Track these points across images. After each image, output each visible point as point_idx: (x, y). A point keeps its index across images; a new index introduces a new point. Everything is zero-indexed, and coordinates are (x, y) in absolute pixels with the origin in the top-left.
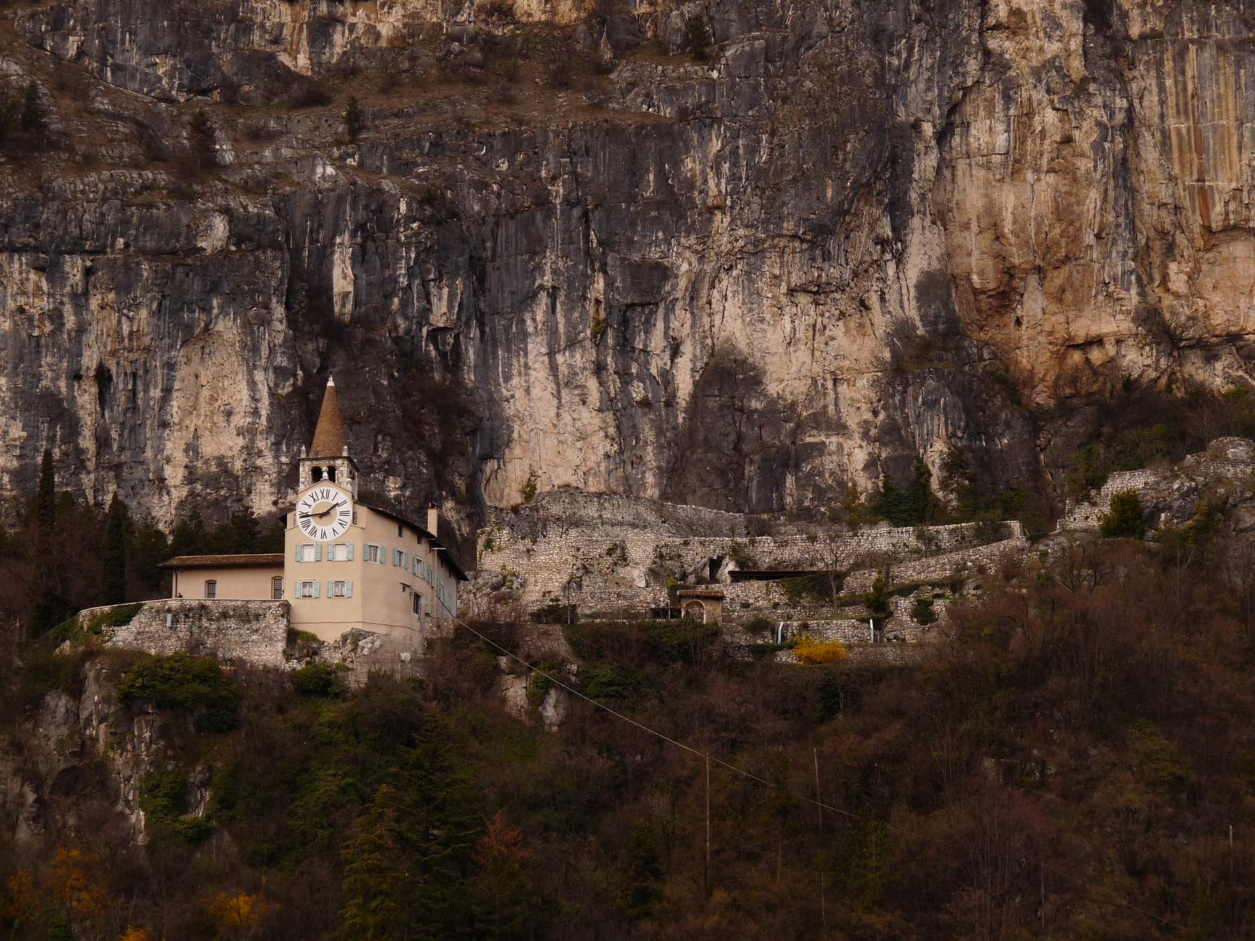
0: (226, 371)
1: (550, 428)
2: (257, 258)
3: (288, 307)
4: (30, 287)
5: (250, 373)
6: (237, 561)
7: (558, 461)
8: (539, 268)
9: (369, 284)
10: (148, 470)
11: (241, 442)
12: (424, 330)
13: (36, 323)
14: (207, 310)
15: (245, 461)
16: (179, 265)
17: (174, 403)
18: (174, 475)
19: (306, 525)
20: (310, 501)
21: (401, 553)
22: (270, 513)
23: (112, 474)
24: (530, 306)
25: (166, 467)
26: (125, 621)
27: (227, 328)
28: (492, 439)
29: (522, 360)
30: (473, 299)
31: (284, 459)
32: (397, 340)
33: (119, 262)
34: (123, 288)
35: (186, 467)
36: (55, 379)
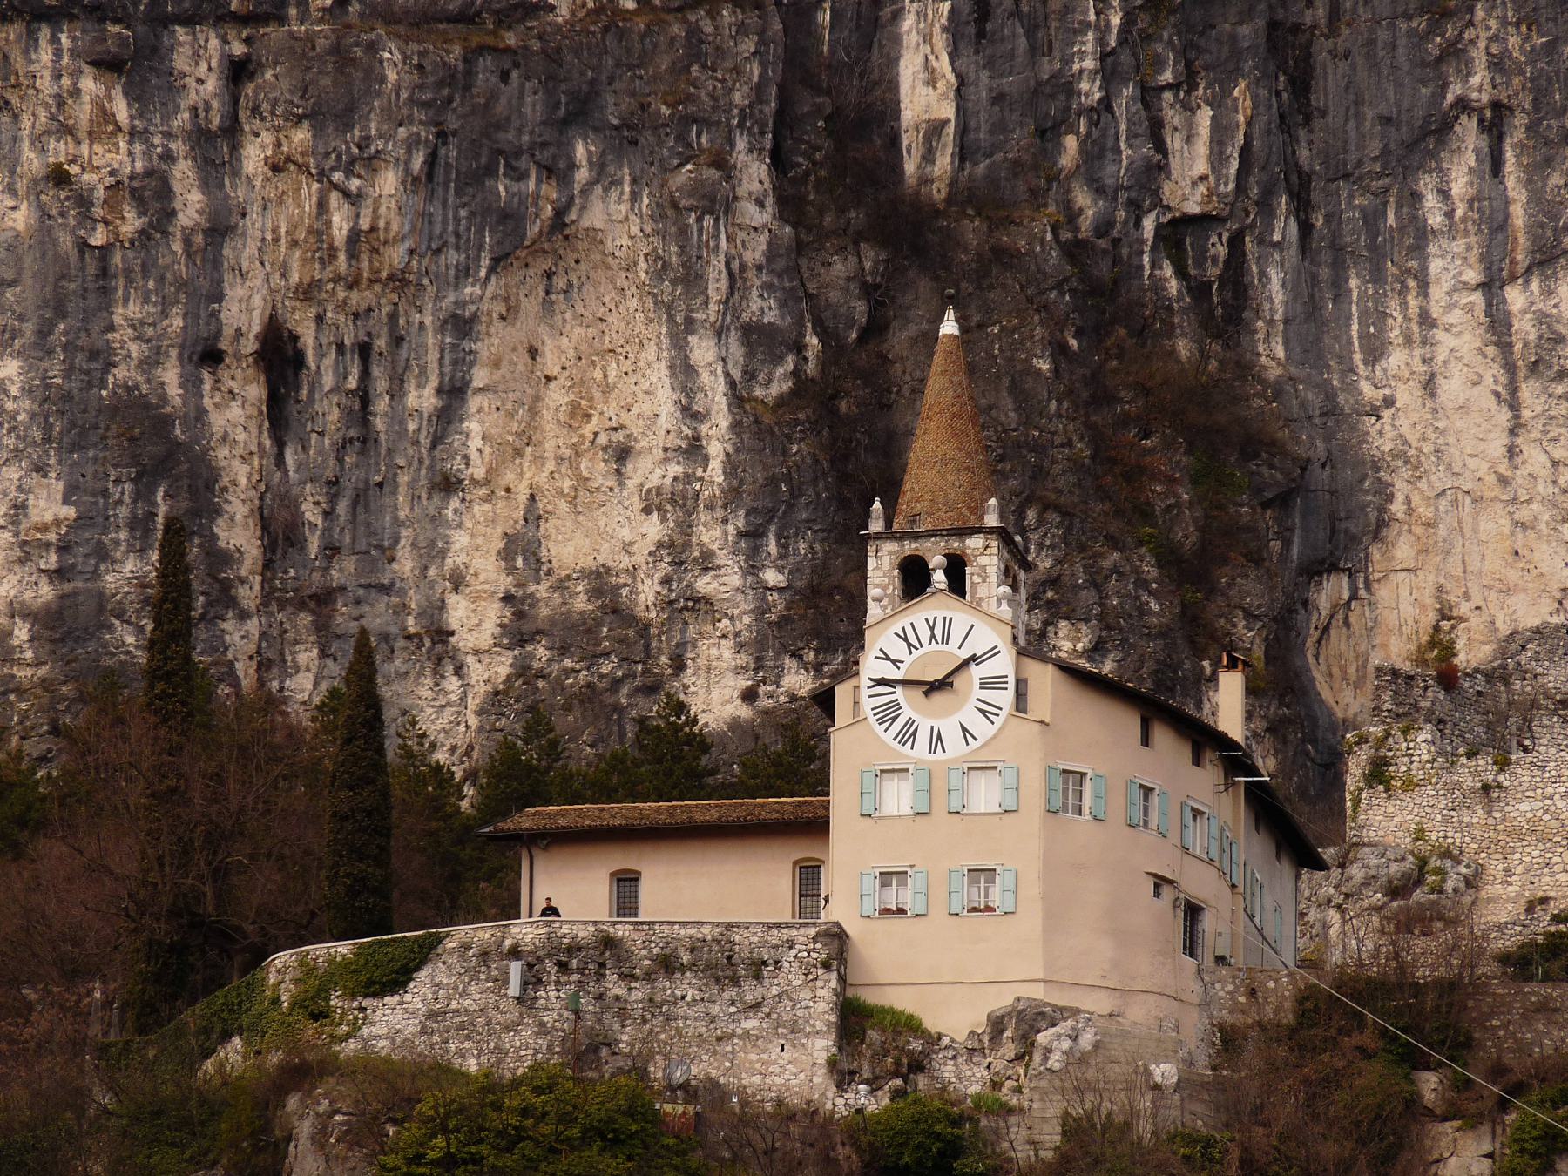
0: (612, 338)
1: (1491, 489)
2: (694, 32)
3: (779, 162)
4: (83, 113)
5: (679, 343)
6: (699, 817)
7: (1513, 575)
8: (1455, 52)
9: (998, 98)
10: (404, 608)
11: (655, 528)
12: (1149, 224)
13: (98, 212)
14: (559, 171)
15: (666, 581)
16: (481, 50)
17: (473, 426)
18: (475, 621)
19: (889, 714)
20: (898, 650)
21: (1147, 791)
22: (735, 724)
23: (305, 619)
24: (1434, 155)
25: (452, 599)
26: (394, 980)
27: (617, 219)
28: (1334, 519)
29: (1413, 303)
30: (1278, 139)
31: (772, 577)
32: (1075, 251)
33: (321, 43)
34: (332, 111)
35: (507, 598)
36: (150, 364)
